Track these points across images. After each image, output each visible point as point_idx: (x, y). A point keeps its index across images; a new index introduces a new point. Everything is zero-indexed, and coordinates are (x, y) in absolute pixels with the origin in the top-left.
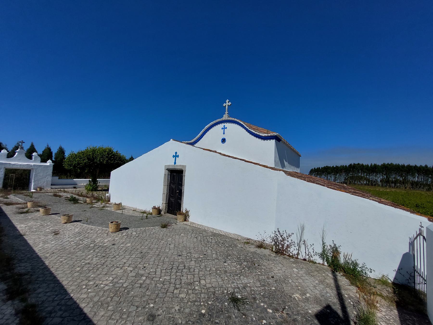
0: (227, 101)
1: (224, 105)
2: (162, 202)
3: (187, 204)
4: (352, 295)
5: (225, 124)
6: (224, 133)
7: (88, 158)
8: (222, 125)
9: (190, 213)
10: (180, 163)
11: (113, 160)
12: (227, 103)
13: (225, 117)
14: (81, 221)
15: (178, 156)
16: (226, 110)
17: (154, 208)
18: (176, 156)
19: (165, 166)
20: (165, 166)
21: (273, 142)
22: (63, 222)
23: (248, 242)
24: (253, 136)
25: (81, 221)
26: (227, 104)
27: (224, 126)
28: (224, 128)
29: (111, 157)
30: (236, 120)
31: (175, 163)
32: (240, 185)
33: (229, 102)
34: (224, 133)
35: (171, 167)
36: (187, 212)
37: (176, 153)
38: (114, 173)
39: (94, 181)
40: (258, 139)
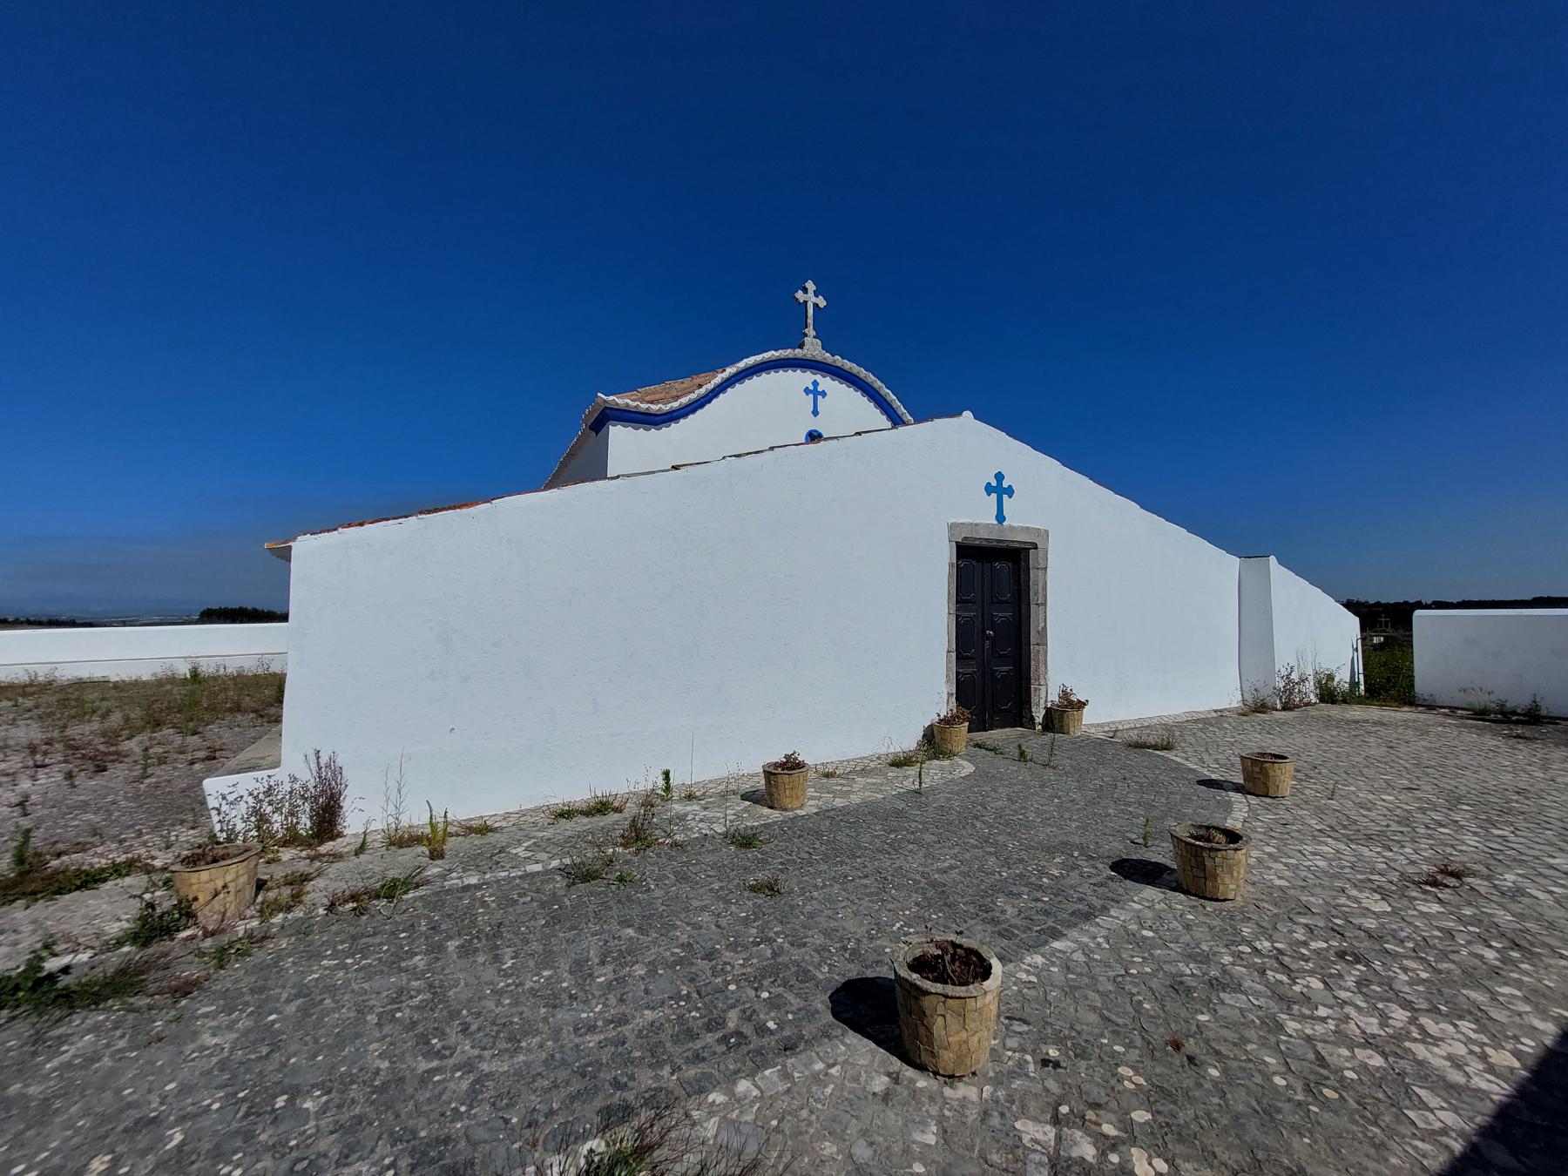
3: (1061, 668)
5: (818, 377)
6: (815, 413)
8: (806, 378)
10: (1021, 518)
14: (1201, 783)
15: (1010, 491)
16: (810, 321)
19: (952, 527)
25: (1201, 783)
27: (815, 383)
31: (1000, 517)
32: (661, 611)
33: (805, 290)
34: (815, 413)
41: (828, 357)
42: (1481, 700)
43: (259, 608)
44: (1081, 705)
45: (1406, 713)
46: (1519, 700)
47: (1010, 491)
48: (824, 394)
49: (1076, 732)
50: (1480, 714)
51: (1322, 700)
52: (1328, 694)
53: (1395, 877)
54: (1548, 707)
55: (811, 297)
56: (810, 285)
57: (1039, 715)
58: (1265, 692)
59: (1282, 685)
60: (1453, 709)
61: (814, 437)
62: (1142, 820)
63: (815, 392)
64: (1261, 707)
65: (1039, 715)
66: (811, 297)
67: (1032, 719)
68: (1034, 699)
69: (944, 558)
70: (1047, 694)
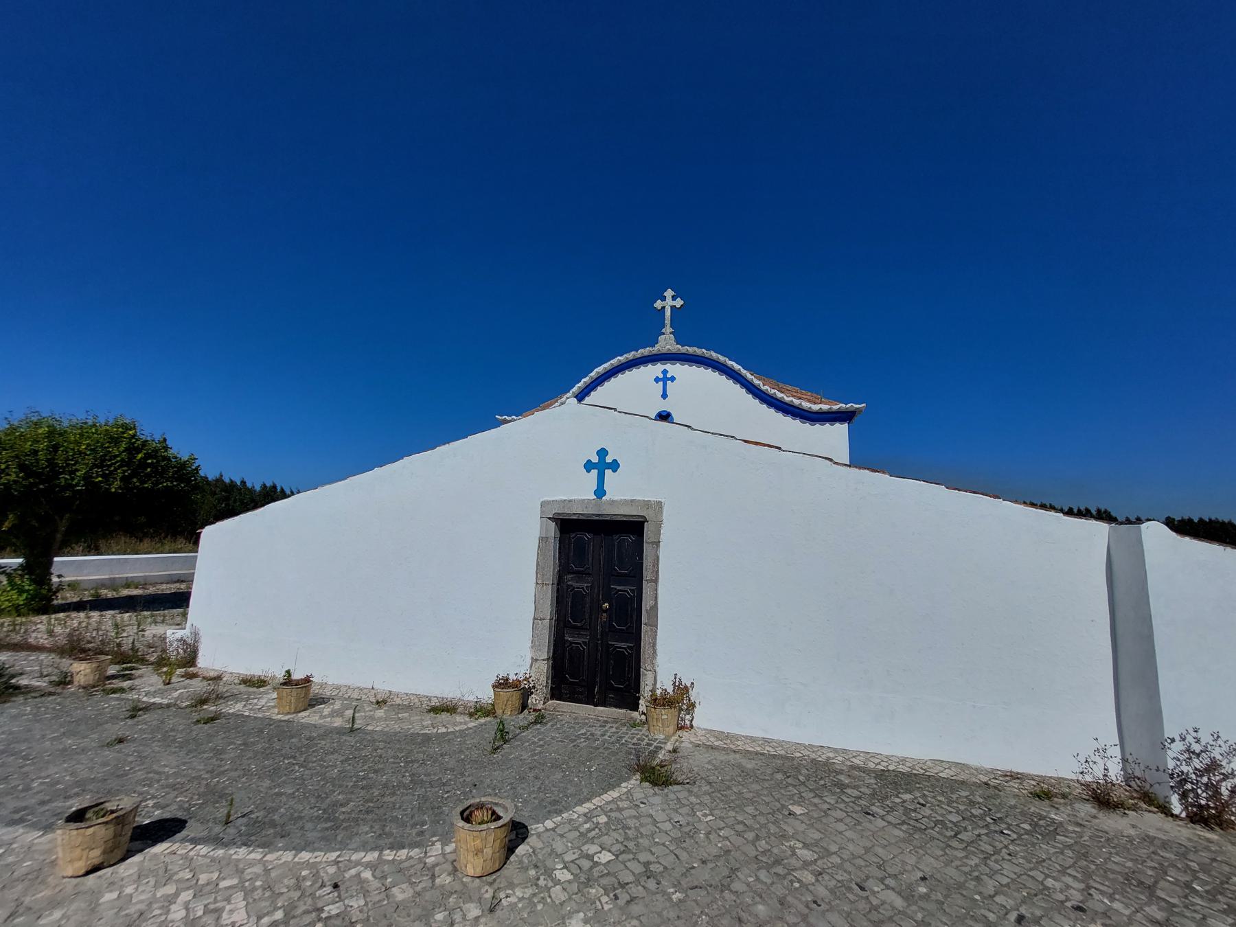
0: (669, 293)
1: (659, 304)
2: (528, 655)
4: (279, 717)
5: (668, 366)
6: (664, 396)
7: (22, 467)
8: (656, 369)
9: (694, 695)
10: (623, 493)
11: (149, 476)
12: (669, 302)
13: (666, 342)
16: (668, 321)
17: (502, 684)
18: (602, 465)
19: (543, 504)
20: (543, 504)
21: (842, 429)
22: (81, 866)
23: (1045, 792)
24: (772, 410)
26: (669, 302)
27: (665, 372)
28: (665, 379)
29: (143, 464)
30: (714, 355)
31: (600, 492)
33: (674, 298)
34: (664, 396)
35: (577, 510)
36: (682, 690)
37: (602, 453)
38: (209, 534)
39: (38, 568)
40: (789, 419)
48: (673, 379)
61: (664, 417)
62: (258, 869)
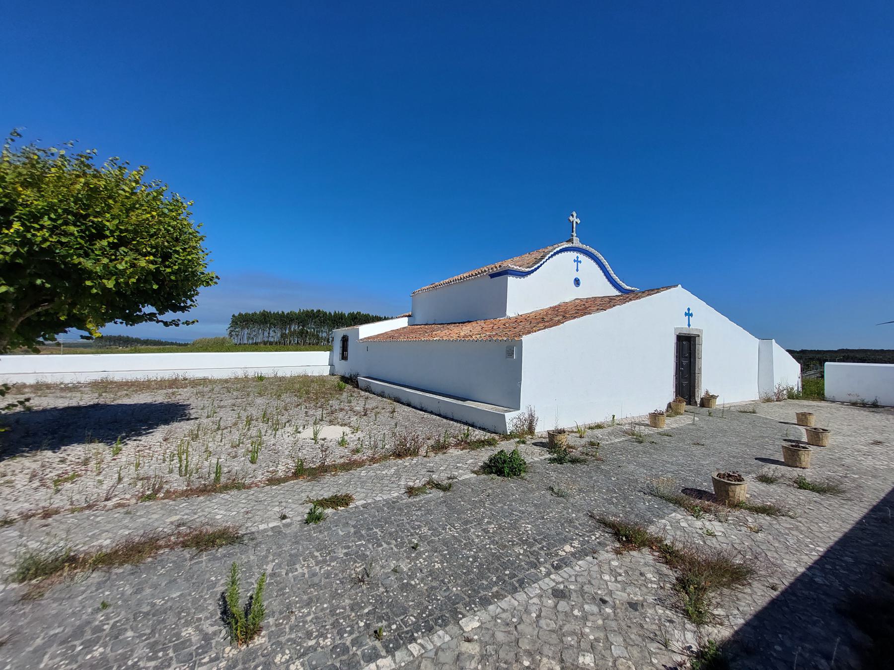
3: (706, 385)
8: (573, 255)
10: (696, 326)
19: (676, 329)
41: (580, 245)
42: (848, 399)
43: (130, 336)
44: (714, 397)
45: (823, 404)
46: (869, 399)
47: (691, 315)
49: (714, 407)
50: (854, 404)
51: (789, 398)
52: (791, 396)
53: (705, 530)
54: (881, 402)
55: (575, 220)
56: (574, 214)
57: (698, 401)
58: (771, 394)
59: (776, 391)
60: (842, 403)
63: (577, 261)
64: (768, 400)
65: (698, 401)
66: (575, 220)
67: (696, 402)
68: (697, 394)
69: (673, 340)
70: (700, 394)
